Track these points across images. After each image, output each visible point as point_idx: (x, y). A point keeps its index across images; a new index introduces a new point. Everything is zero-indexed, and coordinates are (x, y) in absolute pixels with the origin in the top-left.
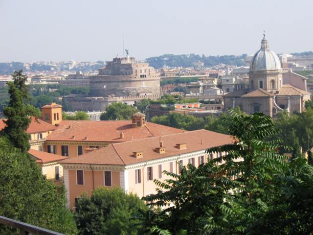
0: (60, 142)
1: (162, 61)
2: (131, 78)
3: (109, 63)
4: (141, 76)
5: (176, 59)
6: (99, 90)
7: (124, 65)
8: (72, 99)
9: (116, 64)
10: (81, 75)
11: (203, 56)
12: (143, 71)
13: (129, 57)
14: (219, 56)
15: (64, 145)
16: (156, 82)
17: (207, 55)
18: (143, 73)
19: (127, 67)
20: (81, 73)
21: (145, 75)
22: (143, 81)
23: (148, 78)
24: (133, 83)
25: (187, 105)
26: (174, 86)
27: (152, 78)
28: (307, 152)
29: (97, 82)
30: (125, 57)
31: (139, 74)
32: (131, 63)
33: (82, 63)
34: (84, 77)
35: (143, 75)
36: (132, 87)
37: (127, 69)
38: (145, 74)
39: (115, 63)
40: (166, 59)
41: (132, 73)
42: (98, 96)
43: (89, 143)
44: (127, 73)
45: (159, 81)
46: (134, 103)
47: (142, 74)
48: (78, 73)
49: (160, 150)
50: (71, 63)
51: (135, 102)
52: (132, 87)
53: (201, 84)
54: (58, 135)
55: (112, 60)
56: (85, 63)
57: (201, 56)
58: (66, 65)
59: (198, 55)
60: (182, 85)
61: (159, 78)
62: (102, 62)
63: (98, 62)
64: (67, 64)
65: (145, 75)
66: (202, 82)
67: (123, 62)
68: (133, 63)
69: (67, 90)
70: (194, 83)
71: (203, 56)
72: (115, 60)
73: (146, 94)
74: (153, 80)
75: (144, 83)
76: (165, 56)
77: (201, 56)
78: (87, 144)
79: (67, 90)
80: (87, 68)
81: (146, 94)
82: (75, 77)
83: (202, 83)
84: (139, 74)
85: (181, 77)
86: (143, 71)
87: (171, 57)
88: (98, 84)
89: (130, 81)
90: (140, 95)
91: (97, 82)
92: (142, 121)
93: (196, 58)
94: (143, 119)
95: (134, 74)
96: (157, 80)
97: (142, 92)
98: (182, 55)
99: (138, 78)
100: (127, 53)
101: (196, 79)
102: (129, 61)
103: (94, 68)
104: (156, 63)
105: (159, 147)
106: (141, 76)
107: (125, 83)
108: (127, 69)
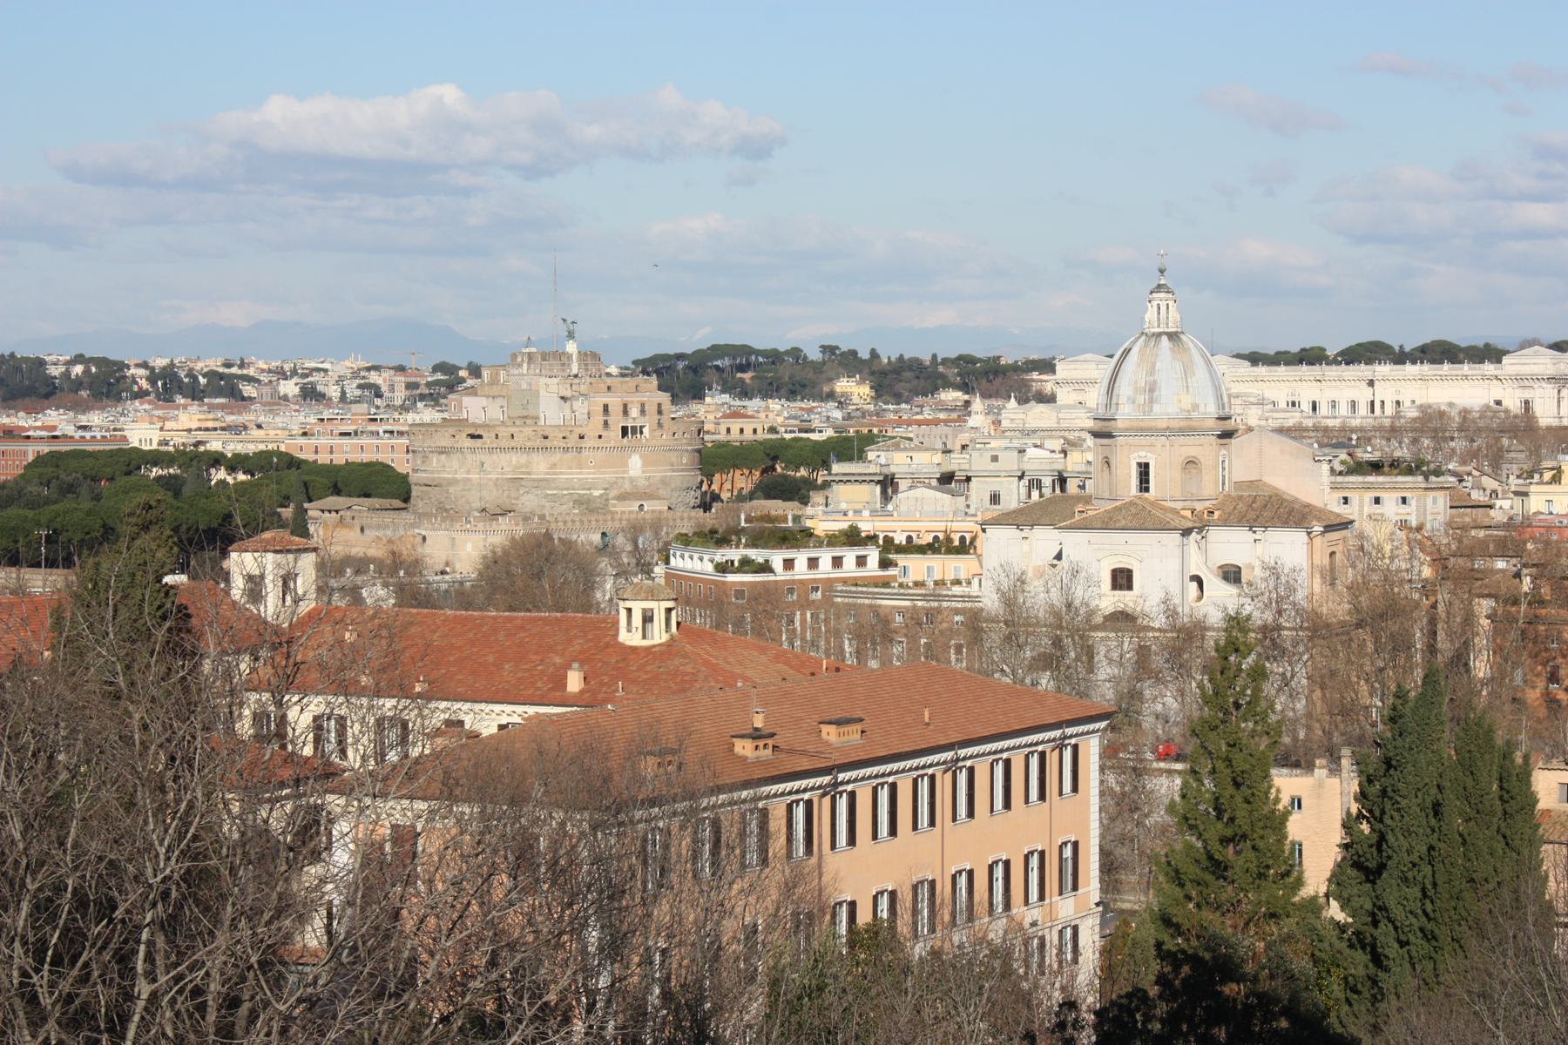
11: (874, 354)
57: (1397, 349)
71: (874, 354)
76: (717, 351)
77: (864, 354)
86: (634, 412)
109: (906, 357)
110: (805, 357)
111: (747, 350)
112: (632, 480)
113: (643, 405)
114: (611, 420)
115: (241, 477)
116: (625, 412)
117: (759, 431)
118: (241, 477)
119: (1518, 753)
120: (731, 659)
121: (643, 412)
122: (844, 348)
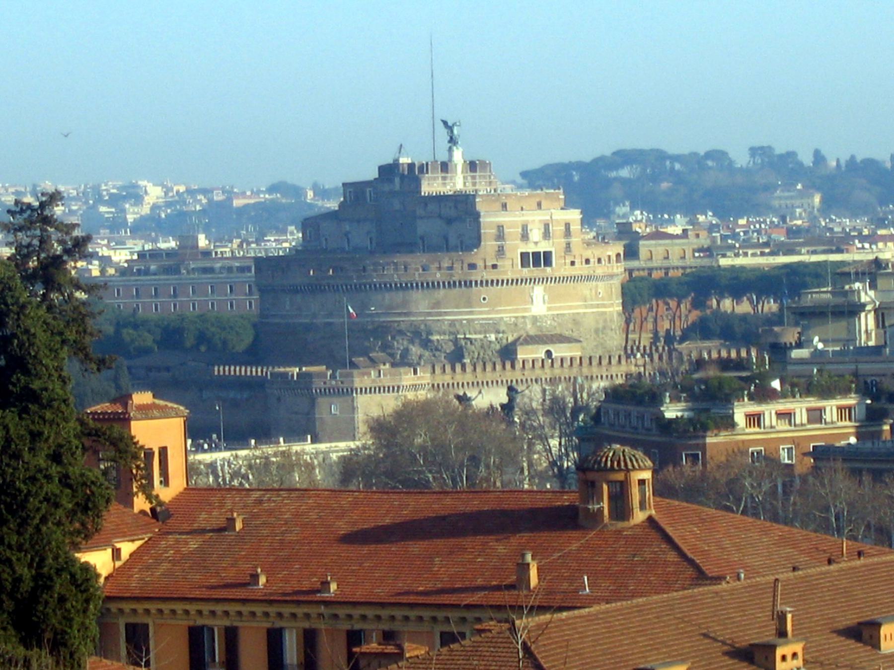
0: (179, 607)
1: (608, 183)
2: (472, 266)
3: (355, 192)
4: (524, 256)
5: (678, 174)
6: (308, 328)
7: (440, 199)
8: (165, 375)
9: (393, 193)
10: (206, 254)
11: (819, 157)
12: (536, 234)
13: (458, 157)
14: (843, 162)
15: (200, 622)
16: (601, 286)
17: (836, 156)
18: (537, 244)
19: (452, 213)
20: (203, 242)
21: (547, 256)
22: (534, 281)
23: (560, 267)
24: (484, 291)
25: (800, 407)
26: (688, 315)
27: (580, 269)
28: (237, 529)
29: (295, 290)
30: (442, 157)
31: (516, 248)
32: (470, 189)
33: (189, 191)
34: (218, 265)
35: (536, 255)
36: (481, 314)
37: (449, 221)
38: (543, 247)
39: (386, 188)
40: (625, 173)
41: (477, 241)
42: (300, 363)
43: (342, 612)
44: (453, 241)
45: (616, 283)
46: (505, 400)
47: (531, 248)
48: (188, 245)
49: (779, 652)
50: (135, 195)
51: (511, 390)
52: (481, 314)
53: (867, 296)
54: (165, 566)
55: (372, 174)
56: (205, 191)
57: (807, 159)
58: (108, 203)
59: (791, 155)
60: (727, 304)
61: (619, 269)
62: (297, 191)
63: (272, 189)
64: (114, 200)
65: (547, 256)
66: (873, 286)
67: (431, 186)
68: (483, 189)
69: (136, 326)
70: (822, 295)
71: (819, 157)
72: (388, 171)
73: (549, 353)
74: (589, 278)
75: (539, 291)
76: (624, 157)
77: (807, 159)
78: (336, 616)
79: (136, 326)
80: (221, 217)
81: (549, 353)
82: (171, 263)
83: (872, 293)
84: (516, 248)
85: (724, 262)
86: (536, 234)
87: (652, 161)
88: (299, 298)
89: (468, 284)
90: (523, 354)
91: (295, 290)
92: (635, 491)
93: (780, 167)
94: (642, 482)
95: (489, 245)
96: (611, 276)
97: (531, 340)
98: (709, 155)
99: (511, 268)
100: (452, 140)
101: (842, 275)
102: (458, 182)
103: (266, 217)
104: (587, 186)
105: (768, 637)
106: (524, 256)
107: (441, 293)
108: (449, 221)
109: (859, 159)
110: (731, 162)
111: (661, 156)
112: (535, 319)
113: (547, 226)
114: (508, 244)
115: (529, 558)
116: (525, 236)
117: (689, 254)
118: (529, 558)
119: (84, 264)
120: (727, 543)
121: (547, 235)
122: (780, 149)
